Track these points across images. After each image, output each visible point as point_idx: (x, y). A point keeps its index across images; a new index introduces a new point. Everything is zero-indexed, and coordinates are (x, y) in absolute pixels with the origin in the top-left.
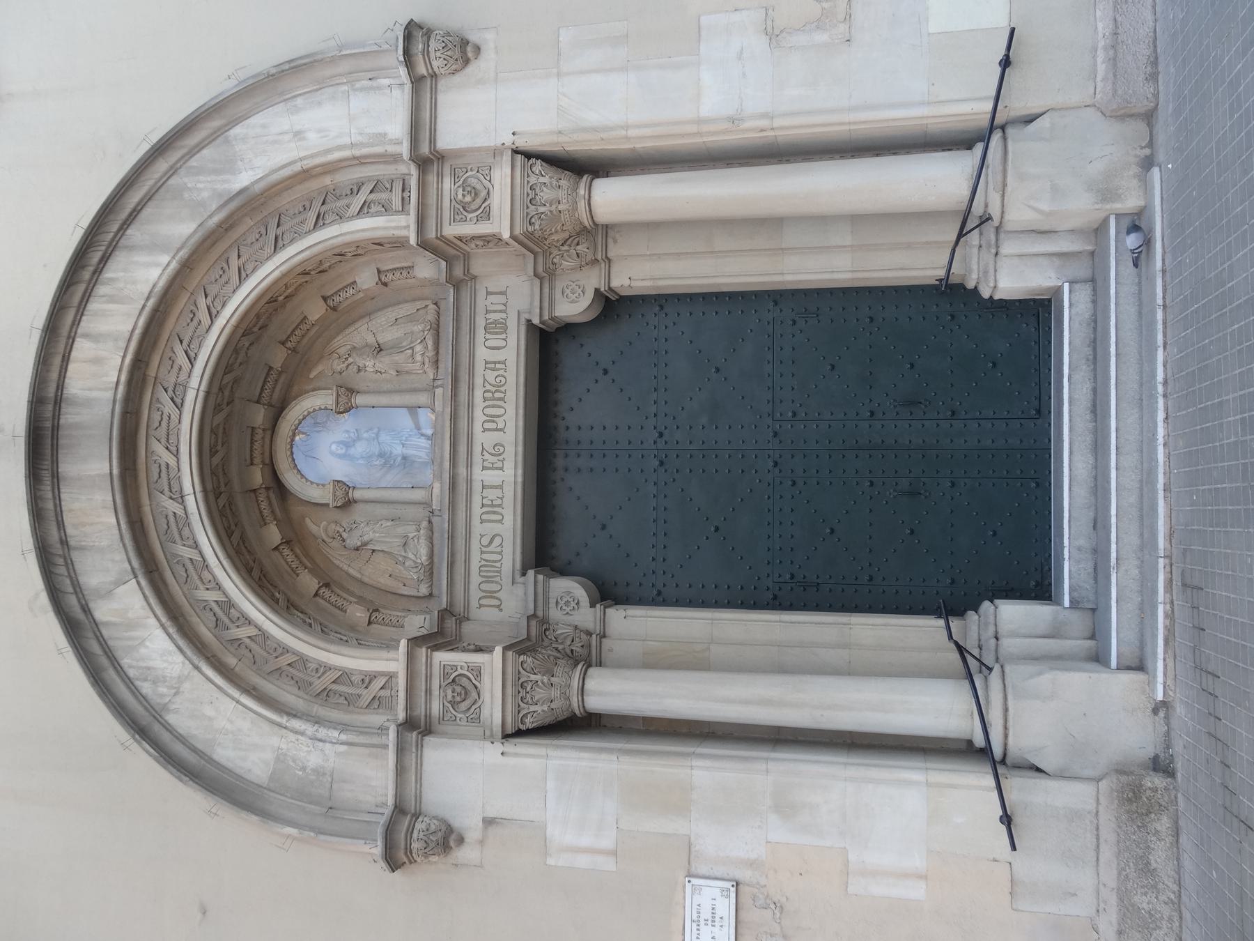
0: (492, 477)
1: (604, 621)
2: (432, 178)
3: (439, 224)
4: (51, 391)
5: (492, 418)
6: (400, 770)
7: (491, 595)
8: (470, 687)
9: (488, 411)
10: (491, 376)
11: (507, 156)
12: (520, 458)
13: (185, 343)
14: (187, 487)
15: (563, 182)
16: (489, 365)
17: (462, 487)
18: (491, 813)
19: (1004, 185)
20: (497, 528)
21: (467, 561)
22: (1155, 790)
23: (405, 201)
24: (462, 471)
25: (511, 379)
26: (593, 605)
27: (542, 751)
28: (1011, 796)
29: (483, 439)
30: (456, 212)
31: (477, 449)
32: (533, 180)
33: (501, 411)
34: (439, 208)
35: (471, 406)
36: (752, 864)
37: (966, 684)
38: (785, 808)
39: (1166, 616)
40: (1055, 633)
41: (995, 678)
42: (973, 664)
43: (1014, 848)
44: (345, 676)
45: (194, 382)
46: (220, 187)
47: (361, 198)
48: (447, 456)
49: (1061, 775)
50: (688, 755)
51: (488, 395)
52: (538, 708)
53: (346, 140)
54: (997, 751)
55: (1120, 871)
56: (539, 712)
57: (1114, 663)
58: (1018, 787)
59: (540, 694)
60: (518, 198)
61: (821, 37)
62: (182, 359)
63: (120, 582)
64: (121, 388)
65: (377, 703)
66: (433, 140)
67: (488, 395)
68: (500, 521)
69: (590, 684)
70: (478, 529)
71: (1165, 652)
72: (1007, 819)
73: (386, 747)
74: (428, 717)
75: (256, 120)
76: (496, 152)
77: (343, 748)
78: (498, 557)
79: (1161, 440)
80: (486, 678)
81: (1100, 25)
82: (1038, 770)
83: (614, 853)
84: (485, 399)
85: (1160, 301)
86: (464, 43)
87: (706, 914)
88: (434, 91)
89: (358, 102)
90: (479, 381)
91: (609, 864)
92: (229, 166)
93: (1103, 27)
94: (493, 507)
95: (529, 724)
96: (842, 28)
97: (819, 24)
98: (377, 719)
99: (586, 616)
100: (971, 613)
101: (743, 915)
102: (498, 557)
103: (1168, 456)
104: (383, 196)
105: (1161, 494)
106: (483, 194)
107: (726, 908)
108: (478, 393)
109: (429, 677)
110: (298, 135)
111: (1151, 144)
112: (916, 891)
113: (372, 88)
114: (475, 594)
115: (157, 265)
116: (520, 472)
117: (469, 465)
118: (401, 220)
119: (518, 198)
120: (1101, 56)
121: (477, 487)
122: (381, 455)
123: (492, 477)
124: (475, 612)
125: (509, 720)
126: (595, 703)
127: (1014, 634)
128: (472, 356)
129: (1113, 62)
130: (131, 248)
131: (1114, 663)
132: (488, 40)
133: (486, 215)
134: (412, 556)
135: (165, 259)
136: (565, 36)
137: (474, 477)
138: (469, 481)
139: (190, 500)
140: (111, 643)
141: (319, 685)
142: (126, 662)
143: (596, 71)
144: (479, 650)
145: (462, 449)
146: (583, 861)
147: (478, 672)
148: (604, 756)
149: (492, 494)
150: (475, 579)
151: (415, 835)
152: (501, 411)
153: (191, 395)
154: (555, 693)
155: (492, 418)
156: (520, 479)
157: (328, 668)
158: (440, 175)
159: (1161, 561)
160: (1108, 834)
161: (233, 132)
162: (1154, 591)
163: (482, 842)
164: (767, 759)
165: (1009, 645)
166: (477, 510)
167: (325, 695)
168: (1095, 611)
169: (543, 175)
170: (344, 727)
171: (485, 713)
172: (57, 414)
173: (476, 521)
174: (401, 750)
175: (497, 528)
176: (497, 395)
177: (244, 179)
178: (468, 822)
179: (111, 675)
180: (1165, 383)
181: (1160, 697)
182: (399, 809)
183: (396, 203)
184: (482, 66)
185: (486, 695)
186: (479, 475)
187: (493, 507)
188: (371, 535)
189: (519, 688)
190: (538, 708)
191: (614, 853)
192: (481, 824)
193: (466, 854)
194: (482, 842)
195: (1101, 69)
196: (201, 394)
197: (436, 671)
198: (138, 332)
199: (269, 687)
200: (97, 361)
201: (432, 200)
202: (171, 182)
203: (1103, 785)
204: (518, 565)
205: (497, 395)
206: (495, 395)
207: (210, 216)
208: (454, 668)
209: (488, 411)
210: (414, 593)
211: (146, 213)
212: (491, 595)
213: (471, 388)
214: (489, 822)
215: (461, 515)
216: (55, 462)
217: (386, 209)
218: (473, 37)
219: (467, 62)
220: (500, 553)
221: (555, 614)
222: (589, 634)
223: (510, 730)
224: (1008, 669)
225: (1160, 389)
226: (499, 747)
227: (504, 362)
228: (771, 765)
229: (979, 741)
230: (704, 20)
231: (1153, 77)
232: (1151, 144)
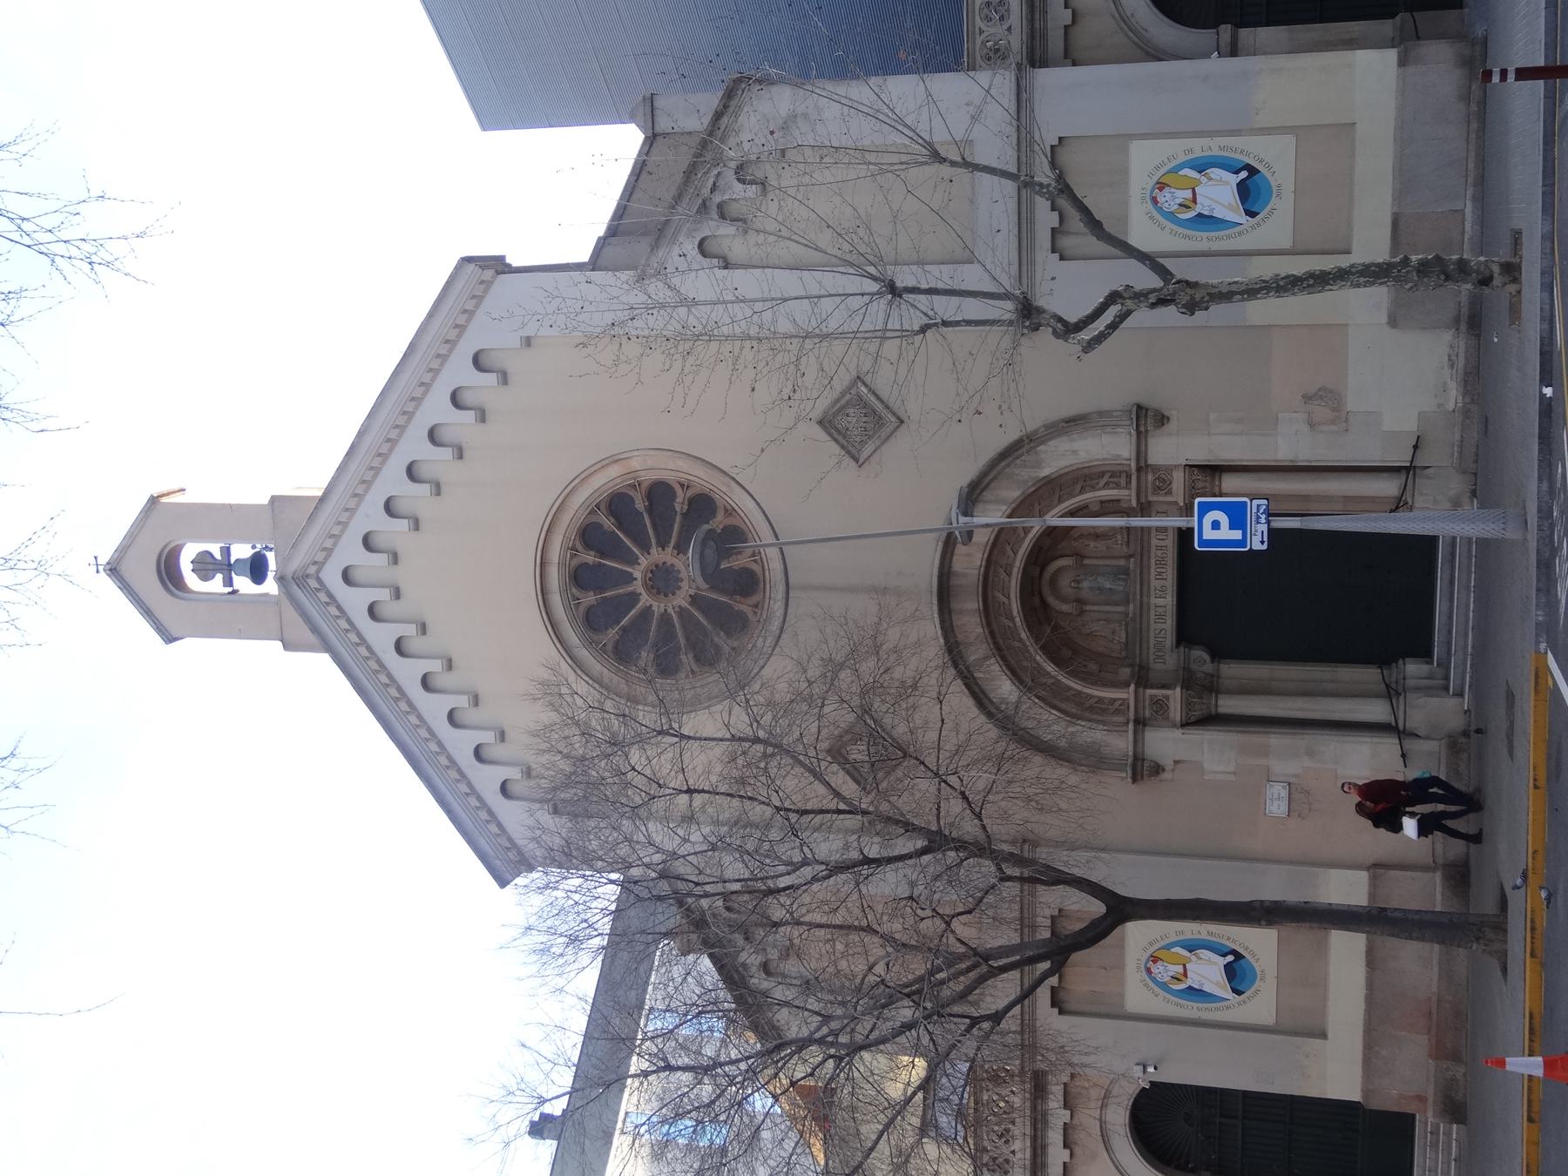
0: (1161, 602)
1: (1218, 670)
2: (1143, 474)
3: (1146, 496)
4: (946, 570)
5: (1160, 574)
6: (1135, 742)
7: (1160, 657)
8: (1163, 704)
9: (1158, 570)
10: (1159, 553)
11: (1182, 469)
12: (1175, 594)
13: (1011, 544)
14: (1015, 613)
15: (1208, 478)
16: (1159, 548)
17: (1145, 607)
18: (1177, 759)
19: (1414, 495)
20: (1164, 626)
21: (1148, 642)
22: (1462, 743)
23: (1129, 482)
24: (1145, 599)
25: (1170, 555)
26: (1212, 662)
27: (1201, 732)
28: (1406, 747)
29: (1155, 583)
30: (1155, 490)
31: (1152, 589)
32: (1194, 477)
33: (1165, 570)
34: (1147, 488)
35: (1149, 568)
36: (1295, 776)
37: (1388, 700)
38: (1310, 753)
39: (1470, 677)
40: (1430, 677)
41: (1401, 698)
42: (1392, 692)
43: (1406, 767)
44: (1101, 700)
45: (1017, 564)
46: (1033, 475)
47: (1102, 482)
48: (1138, 592)
49: (1427, 738)
50: (1268, 732)
51: (1158, 562)
52: (1196, 713)
53: (1100, 457)
54: (1401, 728)
55: (1447, 773)
56: (1197, 714)
57: (1451, 693)
58: (1410, 744)
59: (1197, 707)
60: (1187, 486)
61: (1334, 428)
62: (1010, 552)
63: (986, 658)
64: (982, 569)
65: (1117, 712)
66: (1146, 460)
67: (1158, 562)
68: (1164, 623)
69: (1220, 702)
70: (1153, 626)
71: (1469, 691)
72: (1403, 756)
73: (1127, 731)
74: (1144, 718)
75: (1052, 443)
76: (1176, 466)
77: (1106, 732)
78: (1163, 640)
79: (1471, 609)
80: (1171, 701)
81: (1456, 436)
82: (1417, 735)
83: (1235, 773)
84: (1156, 564)
85: (1474, 554)
86: (1163, 416)
87: (1276, 796)
88: (1146, 438)
89: (1106, 439)
90: (1153, 555)
91: (1232, 778)
92: (1038, 465)
93: (1458, 437)
94: (1161, 616)
95: (1193, 720)
96: (1344, 424)
97: (1333, 422)
98: (1121, 719)
99: (1209, 667)
100: (1394, 664)
101: (1292, 796)
102: (1163, 640)
103: (1474, 617)
104: (1116, 480)
105: (1470, 630)
106: (1168, 482)
107: (1284, 793)
108: (1153, 561)
109: (1144, 701)
110: (1075, 452)
111: (1475, 484)
112: (1232, 778)
113: (1112, 433)
114: (1152, 657)
115: (1001, 510)
116: (1175, 599)
117: (1149, 596)
118: (1126, 492)
119: (1187, 486)
120: (1456, 449)
121: (1153, 607)
122: (1099, 589)
123: (1161, 602)
124: (1152, 666)
125: (1184, 719)
126: (1221, 710)
127: (1414, 678)
128: (1149, 544)
129: (1460, 453)
130: (986, 502)
131: (1451, 693)
132: (1173, 414)
133: (1170, 493)
134: (1117, 639)
135: (1004, 508)
136: (1212, 416)
137: (1151, 601)
138: (1149, 603)
139: (1017, 619)
140: (983, 687)
141: (1088, 704)
142: (991, 696)
143: (1228, 434)
144: (1163, 687)
145: (1145, 588)
146: (1220, 777)
147: (1167, 698)
148: (1230, 734)
149: (1160, 610)
150: (1152, 650)
151: (1145, 768)
152: (1165, 570)
153: (1015, 570)
154: (1204, 707)
155: (1160, 574)
156: (1175, 603)
157: (1092, 697)
158: (1146, 473)
159: (1469, 657)
160: (1443, 760)
161: (1039, 449)
162: (1466, 668)
163: (1173, 770)
164: (1303, 734)
165: (1410, 683)
166: (1152, 617)
167: (1091, 709)
168: (1445, 665)
169: (1197, 475)
170: (1104, 723)
171: (1172, 715)
172: (948, 581)
173: (1152, 622)
174: (1135, 733)
175: (1164, 626)
176: (1163, 562)
177: (1046, 472)
178: (1167, 763)
179: (985, 701)
180: (1474, 587)
181: (1466, 708)
182: (1136, 758)
183: (1123, 483)
184: (1172, 426)
185: (1172, 708)
186: (1153, 601)
187: (1161, 616)
188: (1095, 628)
189: (1187, 705)
190: (1196, 713)
191: (1235, 773)
192: (1173, 763)
193: (1165, 776)
194: (1173, 770)
195: (1456, 454)
196: (1021, 570)
197: (1147, 697)
198: (991, 542)
199: (1064, 706)
200: (969, 555)
201: (1143, 484)
202: (1007, 470)
203: (1443, 741)
204: (1174, 643)
205: (1163, 562)
206: (1161, 563)
207: (1028, 488)
208: (1156, 696)
209: (1158, 570)
210: (1118, 655)
211: (992, 485)
212: (1160, 657)
213: (1149, 559)
214: (1176, 762)
215: (1144, 620)
216: (949, 602)
217: (1118, 486)
218: (1166, 413)
219: (1163, 425)
220: (1165, 638)
221: (1194, 666)
222: (1213, 676)
223: (1184, 722)
224: (1407, 694)
225: (1472, 589)
226: (1181, 731)
227: (1166, 546)
228: (1306, 736)
229: (1394, 724)
230: (1280, 415)
231: (1476, 461)
232: (1475, 484)
